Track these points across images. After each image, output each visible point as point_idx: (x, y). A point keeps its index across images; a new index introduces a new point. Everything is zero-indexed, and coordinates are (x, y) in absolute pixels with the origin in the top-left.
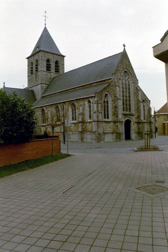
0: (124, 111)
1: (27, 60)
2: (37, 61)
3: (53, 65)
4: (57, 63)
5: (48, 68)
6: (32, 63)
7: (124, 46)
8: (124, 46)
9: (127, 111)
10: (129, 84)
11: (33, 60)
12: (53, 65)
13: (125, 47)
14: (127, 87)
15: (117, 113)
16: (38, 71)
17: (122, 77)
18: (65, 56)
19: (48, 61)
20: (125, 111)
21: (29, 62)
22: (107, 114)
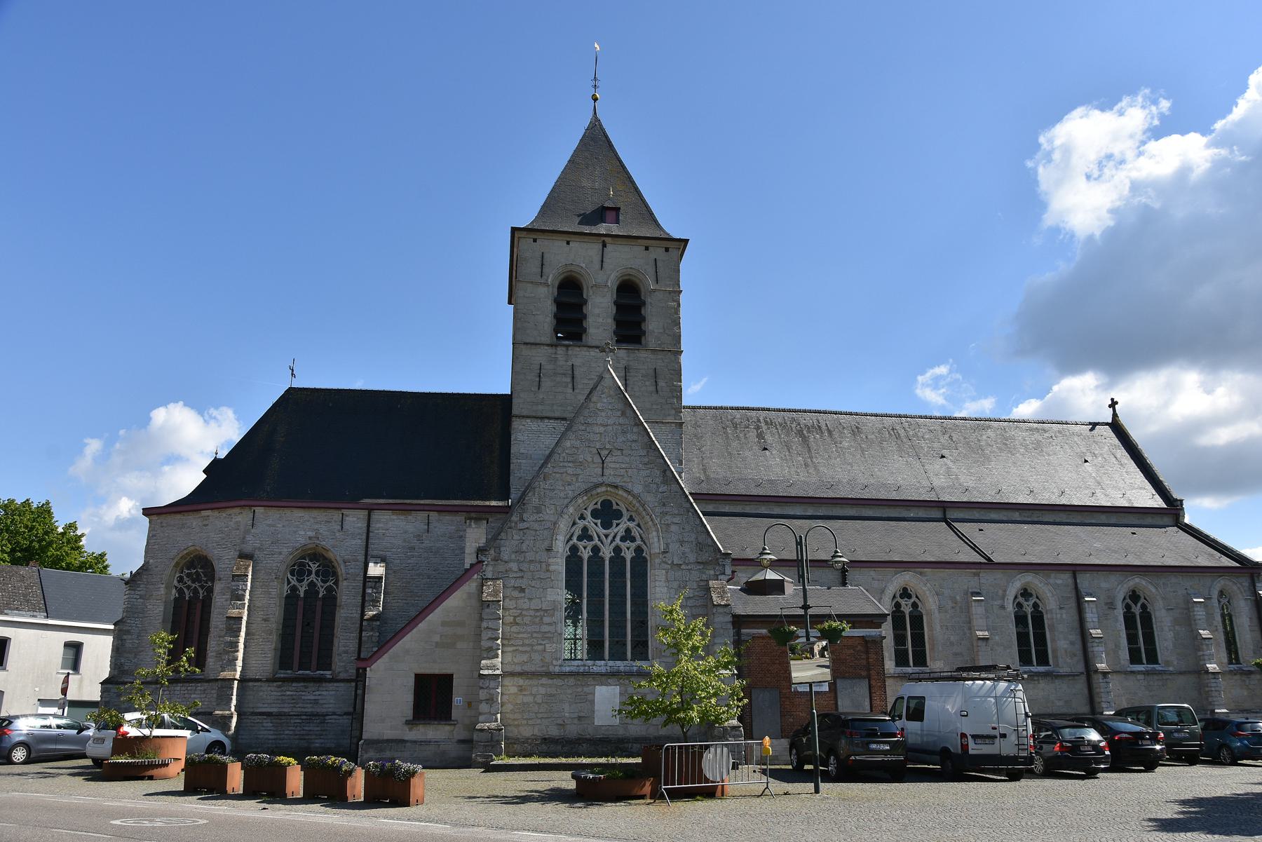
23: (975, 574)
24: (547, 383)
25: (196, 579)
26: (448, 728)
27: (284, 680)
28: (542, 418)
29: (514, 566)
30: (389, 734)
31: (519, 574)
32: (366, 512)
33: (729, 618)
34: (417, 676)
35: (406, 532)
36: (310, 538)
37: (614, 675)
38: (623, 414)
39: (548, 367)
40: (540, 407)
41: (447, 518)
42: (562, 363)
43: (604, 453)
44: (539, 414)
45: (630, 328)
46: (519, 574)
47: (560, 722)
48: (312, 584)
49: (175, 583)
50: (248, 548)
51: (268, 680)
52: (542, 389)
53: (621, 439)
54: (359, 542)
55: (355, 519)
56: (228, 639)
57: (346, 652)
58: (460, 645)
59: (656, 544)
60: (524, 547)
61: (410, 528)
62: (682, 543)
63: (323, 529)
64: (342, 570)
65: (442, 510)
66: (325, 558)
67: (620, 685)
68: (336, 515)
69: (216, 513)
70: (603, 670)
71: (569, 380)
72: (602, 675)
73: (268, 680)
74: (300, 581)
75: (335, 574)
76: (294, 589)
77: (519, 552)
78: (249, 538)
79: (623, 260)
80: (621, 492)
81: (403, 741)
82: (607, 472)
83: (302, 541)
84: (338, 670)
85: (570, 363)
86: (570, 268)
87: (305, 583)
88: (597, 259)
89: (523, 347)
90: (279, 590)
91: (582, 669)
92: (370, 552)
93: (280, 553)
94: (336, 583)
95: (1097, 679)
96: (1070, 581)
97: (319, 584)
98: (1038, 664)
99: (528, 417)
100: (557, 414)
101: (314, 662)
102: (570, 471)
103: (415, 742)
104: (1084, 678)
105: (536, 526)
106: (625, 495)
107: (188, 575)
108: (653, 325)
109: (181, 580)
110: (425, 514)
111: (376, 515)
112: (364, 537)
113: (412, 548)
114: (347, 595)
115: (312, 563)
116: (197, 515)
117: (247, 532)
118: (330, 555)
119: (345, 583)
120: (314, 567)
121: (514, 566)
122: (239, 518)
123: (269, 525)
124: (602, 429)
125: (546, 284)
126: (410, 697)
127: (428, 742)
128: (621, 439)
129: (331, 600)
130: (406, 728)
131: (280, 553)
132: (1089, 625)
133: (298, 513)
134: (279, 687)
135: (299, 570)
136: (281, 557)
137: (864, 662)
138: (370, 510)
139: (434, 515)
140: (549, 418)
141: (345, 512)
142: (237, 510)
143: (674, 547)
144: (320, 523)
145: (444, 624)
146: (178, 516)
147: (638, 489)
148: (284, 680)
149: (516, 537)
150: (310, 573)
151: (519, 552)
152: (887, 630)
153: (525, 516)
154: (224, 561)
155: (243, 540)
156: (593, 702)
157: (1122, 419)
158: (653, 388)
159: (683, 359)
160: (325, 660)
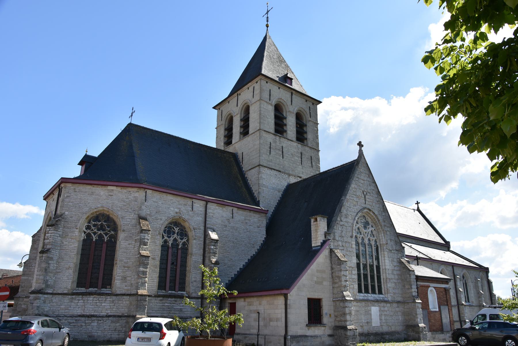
0: (360, 291)
1: (216, 111)
2: (247, 110)
3: (291, 123)
4: (299, 117)
5: (280, 128)
6: (231, 120)
7: (360, 144)
8: (360, 144)
9: (375, 294)
10: (377, 245)
11: (235, 110)
12: (291, 123)
13: (363, 148)
14: (367, 252)
15: (404, 286)
16: (233, 143)
17: (357, 223)
18: (320, 102)
19: (278, 108)
20: (363, 291)
21: (220, 117)
22: (377, 276)
23: (431, 264)
24: (273, 152)
25: (102, 228)
26: (323, 328)
27: (164, 296)
28: (271, 169)
29: (340, 243)
30: (300, 332)
31: (342, 248)
32: (204, 203)
33: (415, 277)
34: (308, 299)
35: (223, 217)
36: (176, 213)
37: (377, 301)
38: (369, 176)
39: (273, 145)
40: (271, 163)
41: (241, 212)
42: (278, 144)
43: (365, 193)
44: (270, 167)
45: (301, 136)
46: (342, 248)
47: (361, 325)
48: (175, 240)
49: (84, 229)
50: (143, 214)
51: (155, 296)
52: (271, 155)
53: (369, 188)
54: (201, 219)
55: (199, 206)
56: (141, 269)
57: (195, 281)
58: (325, 283)
59: (383, 241)
60: (343, 235)
61: (224, 214)
62: (391, 240)
63: (183, 209)
64: (191, 234)
65: (239, 208)
66: (182, 226)
67: (379, 306)
68: (189, 202)
69: (119, 189)
70: (361, 298)
71: (281, 153)
72: (372, 301)
73: (155, 296)
74: (169, 237)
75: (186, 235)
76: (166, 242)
77: (342, 236)
78: (143, 207)
79: (298, 104)
80: (371, 213)
81: (306, 336)
82: (367, 202)
83: (172, 214)
84: (191, 291)
85: (281, 145)
86: (281, 101)
87: (172, 239)
88: (290, 100)
89: (264, 132)
90: (160, 241)
91: (366, 298)
92: (207, 226)
93: (161, 219)
94: (188, 240)
95: (461, 307)
96: (452, 269)
97: (167, 238)
98: (170, 289)
99: (266, 167)
100: (277, 169)
101: (100, 283)
102: (355, 199)
103: (312, 336)
104: (457, 307)
105: (346, 224)
106: (373, 214)
107: (95, 225)
108: (310, 136)
109: (88, 227)
110: (231, 208)
111: (210, 205)
112: (203, 216)
113: (226, 226)
114: (195, 248)
115: (176, 227)
116: (104, 188)
117: (142, 204)
118: (186, 225)
119: (194, 241)
120: (177, 230)
121: (340, 243)
122: (137, 195)
123: (154, 202)
124: (363, 182)
125: (271, 105)
126: (306, 311)
127: (315, 337)
128: (369, 188)
129: (185, 249)
130: (307, 328)
131: (161, 219)
132: (458, 287)
133: (170, 197)
134: (161, 300)
135: (168, 231)
136: (162, 222)
137: (445, 299)
138: (207, 202)
139: (235, 209)
140: (274, 170)
141: (194, 200)
142: (135, 190)
143: (389, 241)
144: (181, 204)
145: (318, 271)
146: (89, 187)
147: (376, 213)
148: (164, 296)
149: (340, 229)
150: (174, 233)
151: (342, 236)
152: (451, 284)
153: (342, 218)
154: (125, 220)
155: (140, 208)
156: (371, 314)
157: (421, 209)
158: (311, 165)
159: (321, 154)
160: (108, 281)
